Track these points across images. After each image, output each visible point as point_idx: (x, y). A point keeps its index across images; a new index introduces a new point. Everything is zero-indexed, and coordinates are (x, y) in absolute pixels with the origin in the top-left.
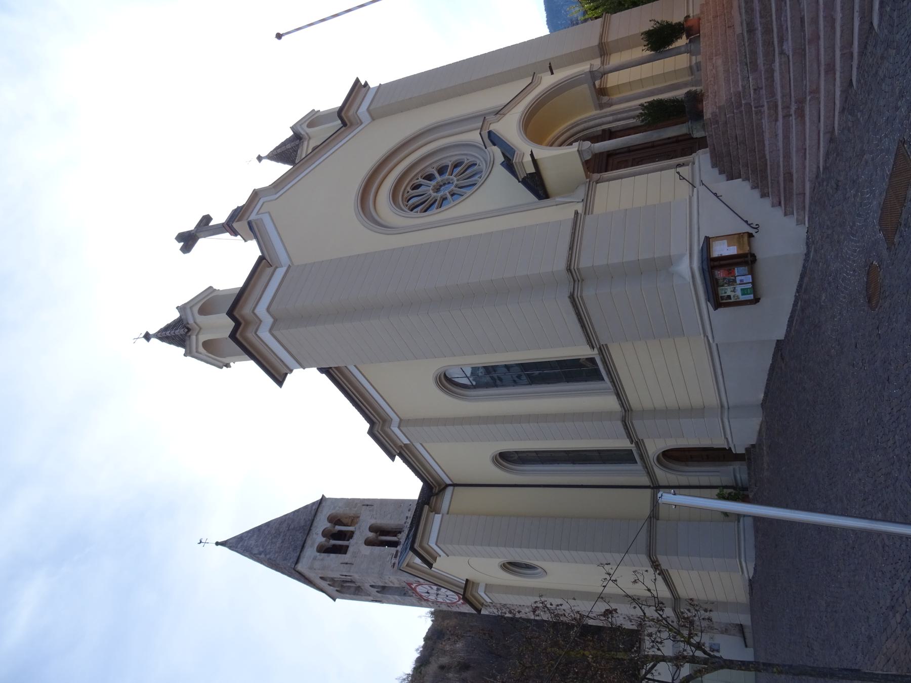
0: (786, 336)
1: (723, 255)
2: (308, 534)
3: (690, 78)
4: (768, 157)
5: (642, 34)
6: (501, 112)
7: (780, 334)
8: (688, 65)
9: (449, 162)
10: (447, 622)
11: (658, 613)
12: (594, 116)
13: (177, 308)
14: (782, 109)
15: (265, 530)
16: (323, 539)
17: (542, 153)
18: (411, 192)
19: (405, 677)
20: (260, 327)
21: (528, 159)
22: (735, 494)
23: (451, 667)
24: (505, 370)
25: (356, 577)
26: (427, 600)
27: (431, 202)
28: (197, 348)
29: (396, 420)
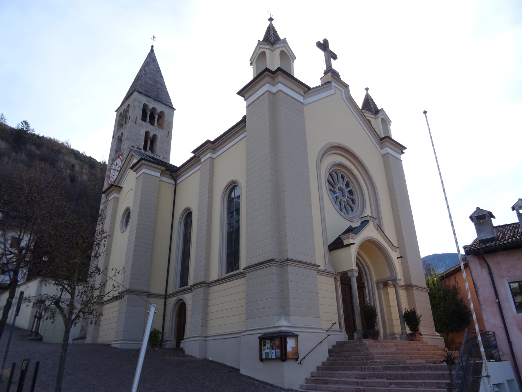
0: (241, 374)
1: (287, 344)
2: (154, 99)
3: (388, 333)
4: (338, 372)
5: (414, 309)
6: (379, 228)
7: (242, 372)
8: (395, 333)
9: (355, 197)
10: (99, 171)
11: (96, 297)
12: (373, 279)
13: (285, 38)
14: (362, 382)
15: (158, 74)
16: (151, 108)
17: (354, 249)
18: (340, 174)
19: (69, 144)
20: (270, 85)
21: (351, 241)
22: (158, 340)
23: (73, 171)
24: (237, 219)
25: (128, 125)
26: (112, 164)
27: (333, 185)
28: (262, 48)
29: (214, 156)
